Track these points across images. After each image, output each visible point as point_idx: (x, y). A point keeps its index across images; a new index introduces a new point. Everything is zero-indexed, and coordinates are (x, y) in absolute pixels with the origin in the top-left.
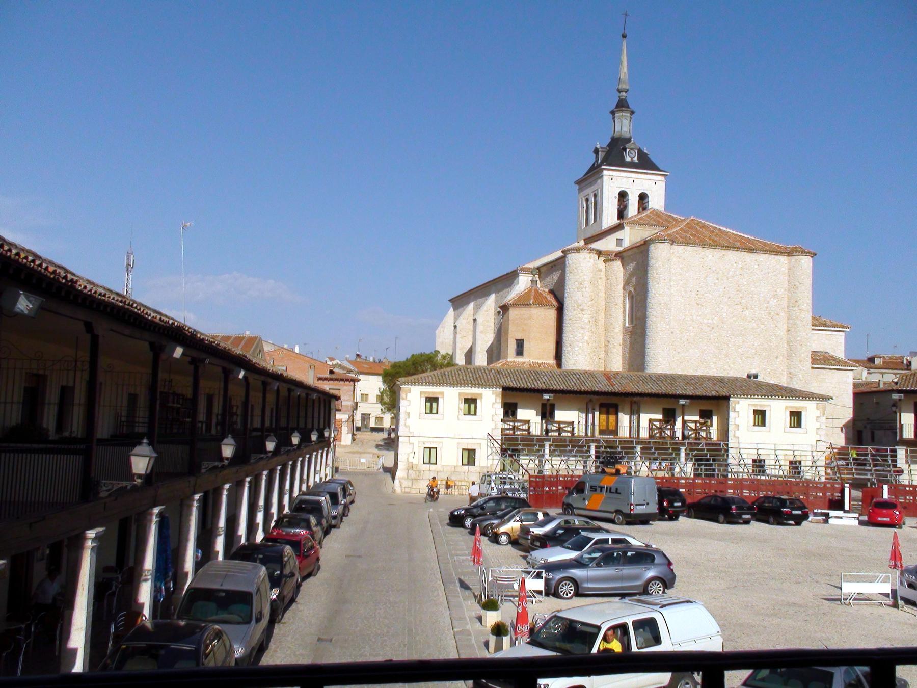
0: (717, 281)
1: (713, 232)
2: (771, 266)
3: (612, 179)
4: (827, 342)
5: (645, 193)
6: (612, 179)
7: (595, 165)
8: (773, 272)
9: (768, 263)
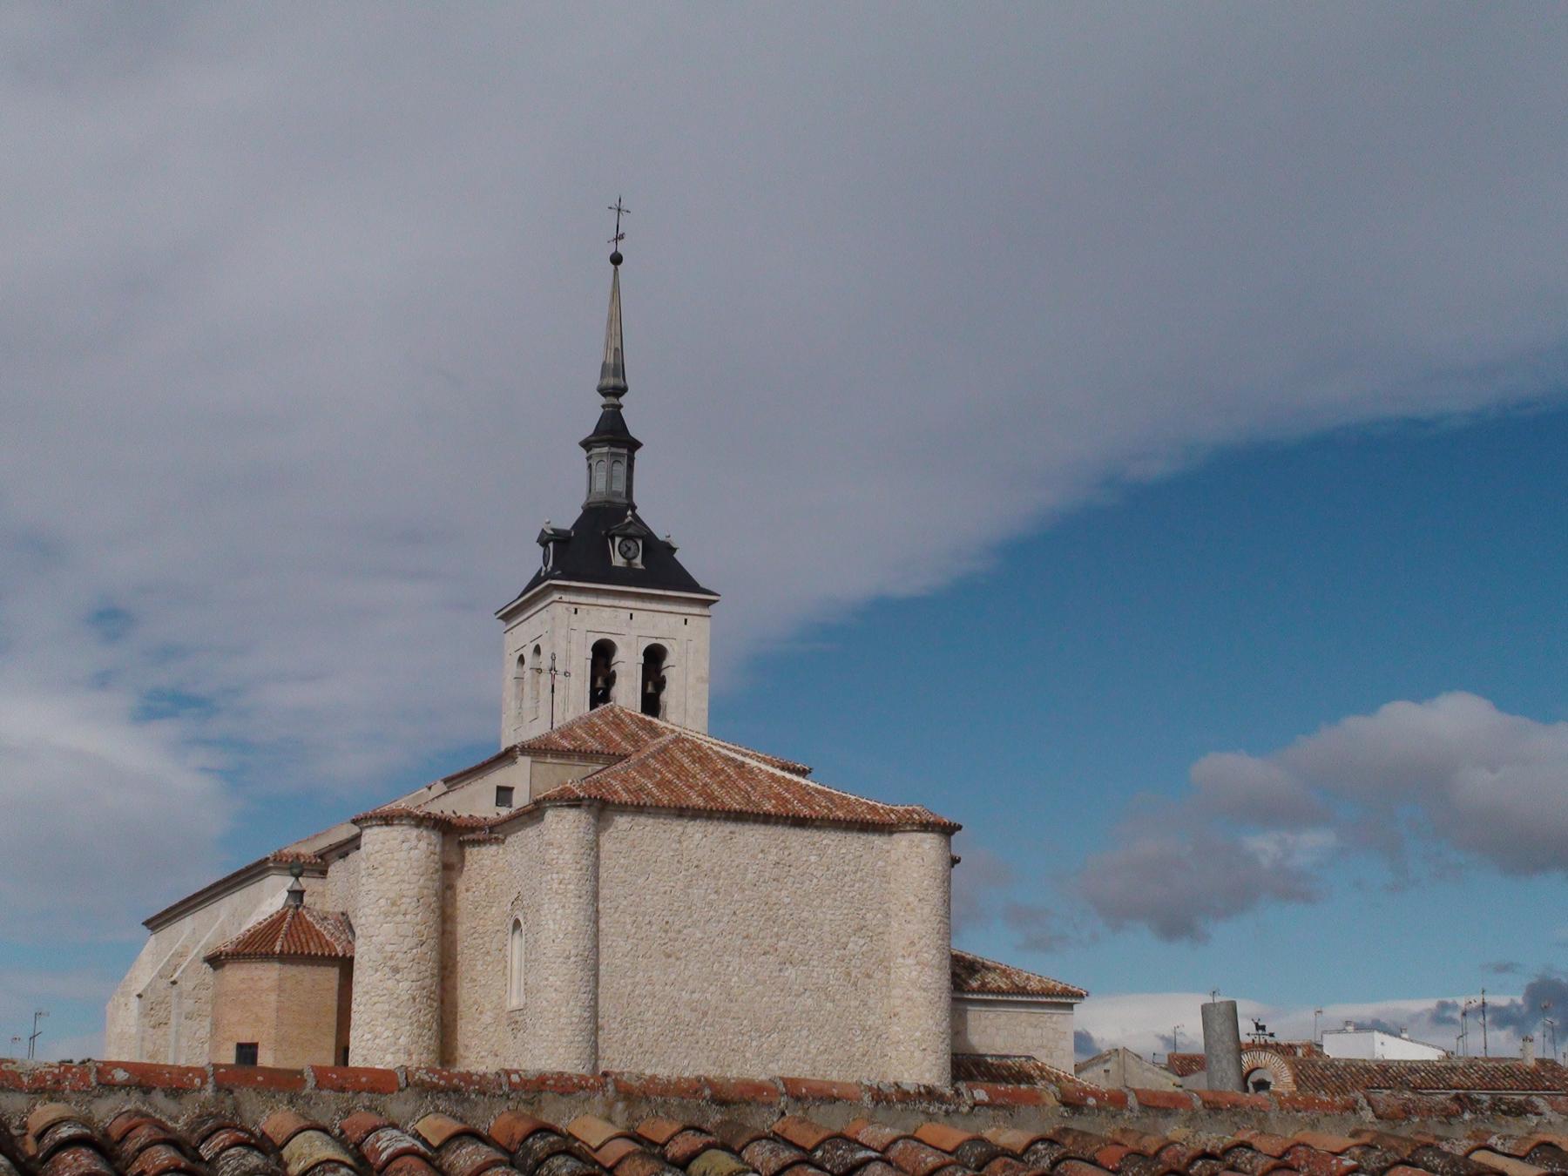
0: (714, 897)
1: (716, 773)
2: (851, 856)
3: (576, 612)
4: (1030, 1031)
5: (645, 651)
6: (576, 612)
7: (542, 574)
8: (856, 872)
9: (844, 851)
